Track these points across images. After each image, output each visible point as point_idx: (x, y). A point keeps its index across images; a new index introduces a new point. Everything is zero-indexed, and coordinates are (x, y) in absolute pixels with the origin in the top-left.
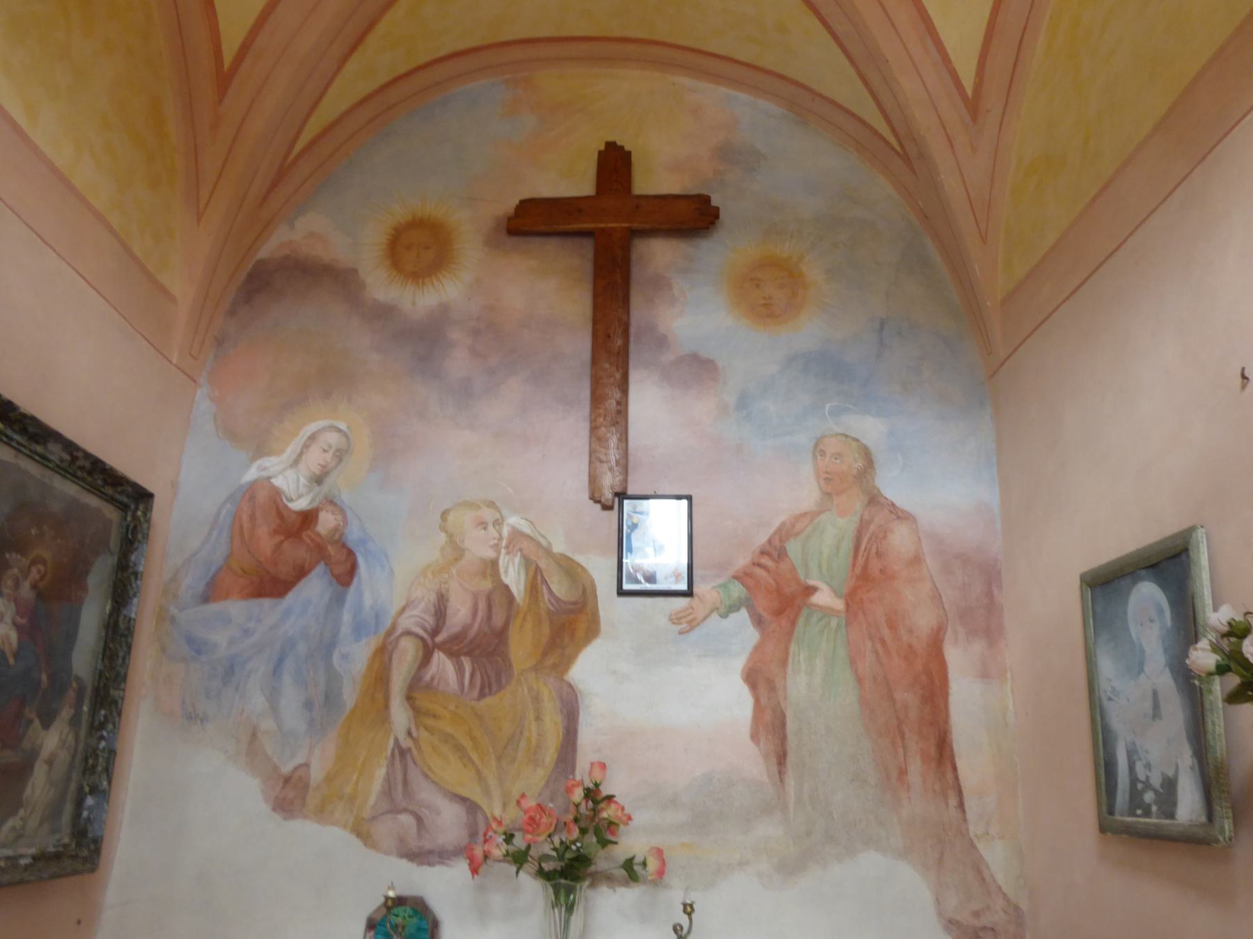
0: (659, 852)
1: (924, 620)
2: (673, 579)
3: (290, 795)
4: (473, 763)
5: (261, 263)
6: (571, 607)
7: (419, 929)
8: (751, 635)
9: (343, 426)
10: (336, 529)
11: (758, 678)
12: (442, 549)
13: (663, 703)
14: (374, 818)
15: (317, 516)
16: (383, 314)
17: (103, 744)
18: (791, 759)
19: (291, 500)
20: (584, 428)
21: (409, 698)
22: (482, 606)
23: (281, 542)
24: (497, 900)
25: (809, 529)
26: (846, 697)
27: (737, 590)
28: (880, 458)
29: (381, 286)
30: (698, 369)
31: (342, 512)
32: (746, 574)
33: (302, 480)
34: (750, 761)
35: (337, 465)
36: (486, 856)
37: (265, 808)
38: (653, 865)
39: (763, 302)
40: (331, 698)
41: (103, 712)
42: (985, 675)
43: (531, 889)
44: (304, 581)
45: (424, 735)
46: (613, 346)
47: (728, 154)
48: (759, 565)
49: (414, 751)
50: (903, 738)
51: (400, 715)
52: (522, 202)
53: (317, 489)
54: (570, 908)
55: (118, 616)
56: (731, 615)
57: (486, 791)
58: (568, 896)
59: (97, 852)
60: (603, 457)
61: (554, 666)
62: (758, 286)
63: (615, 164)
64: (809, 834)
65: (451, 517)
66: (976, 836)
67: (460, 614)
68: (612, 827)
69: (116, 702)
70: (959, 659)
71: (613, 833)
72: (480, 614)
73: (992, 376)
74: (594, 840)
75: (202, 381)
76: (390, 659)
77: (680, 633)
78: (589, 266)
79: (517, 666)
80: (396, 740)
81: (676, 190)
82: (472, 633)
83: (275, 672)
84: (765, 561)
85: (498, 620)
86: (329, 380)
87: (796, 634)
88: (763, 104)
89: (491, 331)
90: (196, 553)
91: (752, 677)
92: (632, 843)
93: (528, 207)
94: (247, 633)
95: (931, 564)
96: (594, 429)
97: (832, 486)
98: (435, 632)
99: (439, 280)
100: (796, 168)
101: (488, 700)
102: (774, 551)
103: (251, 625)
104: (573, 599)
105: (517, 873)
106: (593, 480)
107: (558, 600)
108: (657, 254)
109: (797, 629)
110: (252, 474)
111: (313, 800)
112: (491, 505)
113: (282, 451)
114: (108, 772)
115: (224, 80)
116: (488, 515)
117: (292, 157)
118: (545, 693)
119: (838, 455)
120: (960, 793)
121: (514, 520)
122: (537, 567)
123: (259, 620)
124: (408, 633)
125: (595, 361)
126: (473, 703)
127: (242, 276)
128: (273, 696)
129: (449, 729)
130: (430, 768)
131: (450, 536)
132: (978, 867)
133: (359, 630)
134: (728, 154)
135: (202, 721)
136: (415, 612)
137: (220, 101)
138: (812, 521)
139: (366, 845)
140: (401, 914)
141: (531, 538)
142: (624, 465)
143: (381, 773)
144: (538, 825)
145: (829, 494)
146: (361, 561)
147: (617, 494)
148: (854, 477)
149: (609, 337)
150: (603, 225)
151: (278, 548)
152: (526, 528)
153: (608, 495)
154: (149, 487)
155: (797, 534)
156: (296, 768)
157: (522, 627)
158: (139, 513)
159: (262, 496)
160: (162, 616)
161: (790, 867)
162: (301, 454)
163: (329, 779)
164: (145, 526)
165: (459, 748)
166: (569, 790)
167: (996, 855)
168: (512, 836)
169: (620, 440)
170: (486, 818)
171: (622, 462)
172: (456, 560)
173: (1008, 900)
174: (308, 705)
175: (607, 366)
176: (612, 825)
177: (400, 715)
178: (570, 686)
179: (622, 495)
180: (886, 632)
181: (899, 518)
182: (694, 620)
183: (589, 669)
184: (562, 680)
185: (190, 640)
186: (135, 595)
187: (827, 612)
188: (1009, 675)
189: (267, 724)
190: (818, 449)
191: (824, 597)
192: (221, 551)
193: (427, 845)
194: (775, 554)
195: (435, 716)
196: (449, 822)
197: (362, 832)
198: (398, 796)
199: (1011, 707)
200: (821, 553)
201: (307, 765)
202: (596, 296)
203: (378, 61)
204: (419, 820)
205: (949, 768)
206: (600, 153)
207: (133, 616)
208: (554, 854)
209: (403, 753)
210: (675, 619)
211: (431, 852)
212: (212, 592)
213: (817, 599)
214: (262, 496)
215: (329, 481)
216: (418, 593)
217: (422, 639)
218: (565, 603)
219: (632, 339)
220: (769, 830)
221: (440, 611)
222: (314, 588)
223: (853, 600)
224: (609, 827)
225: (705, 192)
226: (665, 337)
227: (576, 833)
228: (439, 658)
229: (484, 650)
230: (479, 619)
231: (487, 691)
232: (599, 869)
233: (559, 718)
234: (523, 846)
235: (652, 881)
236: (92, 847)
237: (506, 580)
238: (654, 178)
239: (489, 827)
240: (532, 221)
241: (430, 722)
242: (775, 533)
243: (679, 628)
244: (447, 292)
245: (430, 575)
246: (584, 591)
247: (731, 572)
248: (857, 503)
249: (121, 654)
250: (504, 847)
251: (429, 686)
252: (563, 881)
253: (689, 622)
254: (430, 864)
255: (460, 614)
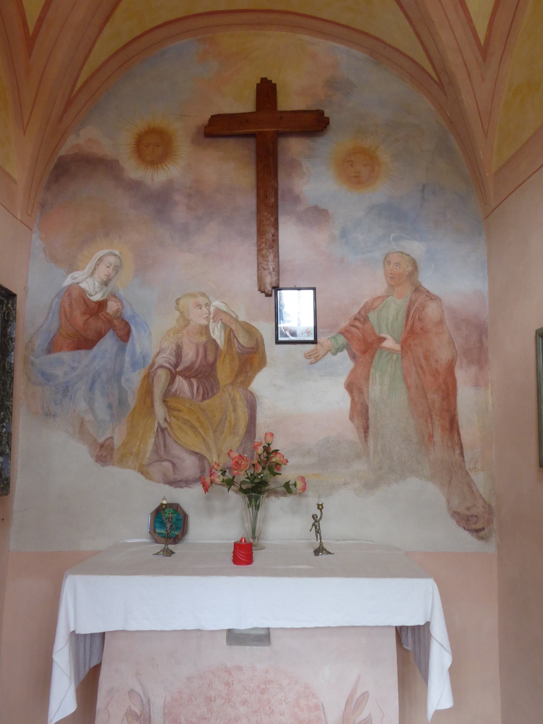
0: (303, 479)
1: (444, 355)
2: (306, 334)
3: (104, 454)
4: (201, 434)
5: (61, 158)
6: (250, 350)
7: (178, 520)
8: (349, 364)
9: (117, 253)
10: (118, 311)
11: (353, 387)
12: (178, 320)
13: (302, 402)
14: (149, 465)
15: (107, 303)
16: (135, 186)
17: (4, 430)
18: (371, 429)
19: (92, 296)
20: (254, 250)
21: (164, 401)
22: (201, 351)
23: (89, 318)
24: (217, 504)
25: (381, 306)
26: (400, 398)
27: (342, 340)
28: (421, 265)
29: (133, 170)
30: (318, 215)
31: (120, 301)
32: (346, 331)
33: (97, 284)
34: (350, 431)
35: (116, 275)
36: (212, 482)
37: (92, 460)
38: (300, 485)
39: (355, 175)
40: (122, 402)
41: (2, 413)
42: (477, 385)
43: (236, 499)
44: (101, 340)
45: (173, 420)
46: (268, 203)
47: (334, 84)
48: (354, 326)
49: (169, 429)
50: (431, 419)
51: (160, 410)
52: (212, 116)
53: (105, 289)
54: (257, 507)
55: (4, 362)
56: (339, 354)
57: (209, 449)
58: (256, 501)
59: (8, 484)
60: (266, 267)
61: (242, 383)
62: (352, 165)
63: (266, 91)
64: (381, 468)
65: (181, 302)
66: (469, 469)
67: (189, 355)
68: (278, 466)
69: (9, 408)
70: (463, 376)
71: (278, 469)
72: (200, 355)
73: (486, 218)
74: (269, 472)
75: (35, 229)
76: (153, 380)
77: (311, 364)
78: (253, 155)
79: (222, 384)
80: (159, 424)
81: (302, 107)
82: (197, 366)
83: (90, 389)
84: (357, 323)
85: (210, 358)
86: (107, 226)
87: (374, 363)
88: (355, 52)
89: (197, 194)
90: (41, 327)
91: (350, 387)
92: (288, 474)
93: (216, 119)
94: (73, 369)
95: (449, 324)
96: (259, 251)
97: (394, 281)
98: (176, 366)
99: (166, 165)
100: (373, 93)
101: (206, 402)
102: (362, 318)
103: (75, 365)
104: (251, 346)
105: (228, 490)
106: (260, 279)
107: (242, 346)
108: (293, 147)
109: (374, 361)
110: (68, 281)
111: (116, 456)
112: (203, 295)
113: (84, 268)
114: (9, 443)
115: (30, 41)
116: (202, 300)
117: (75, 91)
118: (238, 397)
119: (398, 264)
120: (461, 447)
121: (216, 303)
122: (231, 329)
123: (79, 362)
124: (161, 367)
125: (259, 211)
126: (200, 403)
127: (52, 166)
128: (91, 402)
129: (187, 417)
130: (178, 438)
131: (182, 313)
132: (470, 485)
133: (134, 366)
134: (334, 84)
135: (54, 416)
136: (164, 355)
137: (30, 56)
138: (383, 301)
139: (146, 478)
140: (168, 513)
141: (227, 313)
142: (277, 271)
143: (152, 441)
144: (240, 466)
145: (393, 286)
146: (133, 328)
147: (274, 288)
148: (406, 277)
149: (267, 197)
150: (261, 130)
151: (86, 322)
152: (224, 308)
153: (269, 288)
154: (14, 291)
155: (375, 309)
156: (106, 440)
157: (223, 361)
158: (10, 305)
159: (75, 293)
160: (26, 361)
161: (370, 486)
162: (95, 269)
163: (124, 444)
164: (13, 312)
165: (193, 427)
166: (255, 448)
167: (479, 479)
168: (225, 472)
169: (275, 256)
170: (209, 463)
171: (276, 269)
172: (186, 326)
173: (485, 502)
174: (110, 406)
175: (266, 214)
176: (278, 465)
177: (160, 410)
178: (251, 393)
179: (277, 288)
180: (423, 361)
181: (431, 299)
182: (317, 356)
183: (261, 384)
184: (247, 390)
185: (43, 374)
186: (12, 351)
187: (391, 351)
188: (490, 385)
189: (89, 417)
190: (386, 260)
191: (389, 343)
192: (55, 325)
193: (179, 478)
194: (362, 319)
195: (179, 411)
196: (189, 465)
197: (143, 471)
198: (161, 453)
199: (490, 402)
200: (388, 319)
201: (112, 438)
202: (258, 173)
203: (123, 27)
204: (174, 465)
205: (456, 433)
206: (257, 84)
207: (12, 362)
208: (248, 480)
209: (163, 430)
210: (308, 356)
211: (181, 481)
212: (52, 347)
213: (386, 344)
214: (75, 293)
215: (111, 284)
216: (165, 345)
217: (170, 370)
218: (247, 348)
219: (279, 198)
220: (360, 466)
221: (178, 354)
222: (108, 343)
223: (406, 344)
224: (276, 466)
225: (321, 109)
226: (298, 196)
227: (260, 470)
228: (179, 379)
229: (203, 375)
230: (200, 358)
231: (206, 396)
232: (270, 488)
233: (246, 410)
234: (231, 477)
235: (300, 493)
236: (5, 482)
237: (214, 337)
238: (290, 101)
239: (212, 468)
240: (219, 129)
241: (176, 413)
242: (362, 308)
243: (309, 361)
244: (172, 172)
245: (171, 334)
246: (257, 341)
247: (338, 329)
248: (408, 291)
249: (8, 382)
250: (222, 477)
251: (174, 395)
252: (253, 494)
253: (315, 358)
254: (181, 487)
255: (189, 355)
